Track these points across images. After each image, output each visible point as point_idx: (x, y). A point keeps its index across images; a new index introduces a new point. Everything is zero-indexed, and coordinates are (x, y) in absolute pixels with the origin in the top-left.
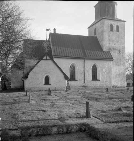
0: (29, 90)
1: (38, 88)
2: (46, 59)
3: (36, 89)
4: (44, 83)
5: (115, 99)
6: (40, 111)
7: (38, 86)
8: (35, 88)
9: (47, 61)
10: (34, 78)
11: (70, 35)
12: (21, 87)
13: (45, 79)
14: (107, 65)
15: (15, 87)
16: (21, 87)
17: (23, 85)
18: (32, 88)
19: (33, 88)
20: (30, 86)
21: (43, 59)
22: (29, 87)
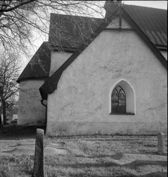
0: (60, 130)
1: (92, 124)
2: (120, 30)
3: (84, 129)
4: (110, 111)
5: (93, 161)
6: (5, 46)
7: (90, 119)
8: (80, 124)
9: (121, 37)
10: (80, 91)
11: (163, 10)
12: (41, 123)
13: (121, 82)
14: (37, 172)
15: (26, 123)
16: (41, 123)
17: (45, 118)
18: (70, 123)
19: (75, 123)
20: (65, 119)
21: (109, 26)
22: (60, 120)
